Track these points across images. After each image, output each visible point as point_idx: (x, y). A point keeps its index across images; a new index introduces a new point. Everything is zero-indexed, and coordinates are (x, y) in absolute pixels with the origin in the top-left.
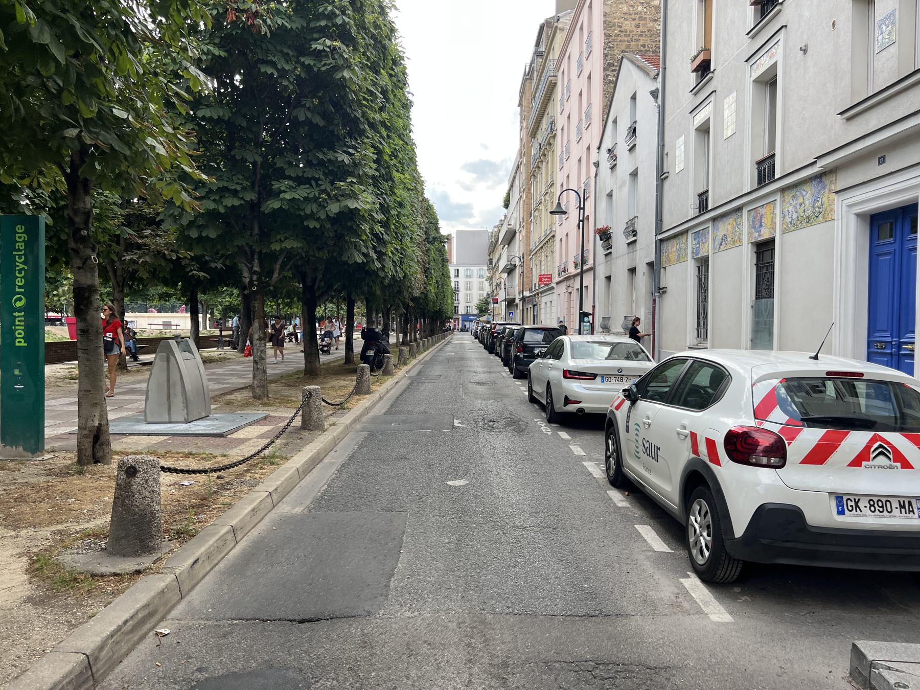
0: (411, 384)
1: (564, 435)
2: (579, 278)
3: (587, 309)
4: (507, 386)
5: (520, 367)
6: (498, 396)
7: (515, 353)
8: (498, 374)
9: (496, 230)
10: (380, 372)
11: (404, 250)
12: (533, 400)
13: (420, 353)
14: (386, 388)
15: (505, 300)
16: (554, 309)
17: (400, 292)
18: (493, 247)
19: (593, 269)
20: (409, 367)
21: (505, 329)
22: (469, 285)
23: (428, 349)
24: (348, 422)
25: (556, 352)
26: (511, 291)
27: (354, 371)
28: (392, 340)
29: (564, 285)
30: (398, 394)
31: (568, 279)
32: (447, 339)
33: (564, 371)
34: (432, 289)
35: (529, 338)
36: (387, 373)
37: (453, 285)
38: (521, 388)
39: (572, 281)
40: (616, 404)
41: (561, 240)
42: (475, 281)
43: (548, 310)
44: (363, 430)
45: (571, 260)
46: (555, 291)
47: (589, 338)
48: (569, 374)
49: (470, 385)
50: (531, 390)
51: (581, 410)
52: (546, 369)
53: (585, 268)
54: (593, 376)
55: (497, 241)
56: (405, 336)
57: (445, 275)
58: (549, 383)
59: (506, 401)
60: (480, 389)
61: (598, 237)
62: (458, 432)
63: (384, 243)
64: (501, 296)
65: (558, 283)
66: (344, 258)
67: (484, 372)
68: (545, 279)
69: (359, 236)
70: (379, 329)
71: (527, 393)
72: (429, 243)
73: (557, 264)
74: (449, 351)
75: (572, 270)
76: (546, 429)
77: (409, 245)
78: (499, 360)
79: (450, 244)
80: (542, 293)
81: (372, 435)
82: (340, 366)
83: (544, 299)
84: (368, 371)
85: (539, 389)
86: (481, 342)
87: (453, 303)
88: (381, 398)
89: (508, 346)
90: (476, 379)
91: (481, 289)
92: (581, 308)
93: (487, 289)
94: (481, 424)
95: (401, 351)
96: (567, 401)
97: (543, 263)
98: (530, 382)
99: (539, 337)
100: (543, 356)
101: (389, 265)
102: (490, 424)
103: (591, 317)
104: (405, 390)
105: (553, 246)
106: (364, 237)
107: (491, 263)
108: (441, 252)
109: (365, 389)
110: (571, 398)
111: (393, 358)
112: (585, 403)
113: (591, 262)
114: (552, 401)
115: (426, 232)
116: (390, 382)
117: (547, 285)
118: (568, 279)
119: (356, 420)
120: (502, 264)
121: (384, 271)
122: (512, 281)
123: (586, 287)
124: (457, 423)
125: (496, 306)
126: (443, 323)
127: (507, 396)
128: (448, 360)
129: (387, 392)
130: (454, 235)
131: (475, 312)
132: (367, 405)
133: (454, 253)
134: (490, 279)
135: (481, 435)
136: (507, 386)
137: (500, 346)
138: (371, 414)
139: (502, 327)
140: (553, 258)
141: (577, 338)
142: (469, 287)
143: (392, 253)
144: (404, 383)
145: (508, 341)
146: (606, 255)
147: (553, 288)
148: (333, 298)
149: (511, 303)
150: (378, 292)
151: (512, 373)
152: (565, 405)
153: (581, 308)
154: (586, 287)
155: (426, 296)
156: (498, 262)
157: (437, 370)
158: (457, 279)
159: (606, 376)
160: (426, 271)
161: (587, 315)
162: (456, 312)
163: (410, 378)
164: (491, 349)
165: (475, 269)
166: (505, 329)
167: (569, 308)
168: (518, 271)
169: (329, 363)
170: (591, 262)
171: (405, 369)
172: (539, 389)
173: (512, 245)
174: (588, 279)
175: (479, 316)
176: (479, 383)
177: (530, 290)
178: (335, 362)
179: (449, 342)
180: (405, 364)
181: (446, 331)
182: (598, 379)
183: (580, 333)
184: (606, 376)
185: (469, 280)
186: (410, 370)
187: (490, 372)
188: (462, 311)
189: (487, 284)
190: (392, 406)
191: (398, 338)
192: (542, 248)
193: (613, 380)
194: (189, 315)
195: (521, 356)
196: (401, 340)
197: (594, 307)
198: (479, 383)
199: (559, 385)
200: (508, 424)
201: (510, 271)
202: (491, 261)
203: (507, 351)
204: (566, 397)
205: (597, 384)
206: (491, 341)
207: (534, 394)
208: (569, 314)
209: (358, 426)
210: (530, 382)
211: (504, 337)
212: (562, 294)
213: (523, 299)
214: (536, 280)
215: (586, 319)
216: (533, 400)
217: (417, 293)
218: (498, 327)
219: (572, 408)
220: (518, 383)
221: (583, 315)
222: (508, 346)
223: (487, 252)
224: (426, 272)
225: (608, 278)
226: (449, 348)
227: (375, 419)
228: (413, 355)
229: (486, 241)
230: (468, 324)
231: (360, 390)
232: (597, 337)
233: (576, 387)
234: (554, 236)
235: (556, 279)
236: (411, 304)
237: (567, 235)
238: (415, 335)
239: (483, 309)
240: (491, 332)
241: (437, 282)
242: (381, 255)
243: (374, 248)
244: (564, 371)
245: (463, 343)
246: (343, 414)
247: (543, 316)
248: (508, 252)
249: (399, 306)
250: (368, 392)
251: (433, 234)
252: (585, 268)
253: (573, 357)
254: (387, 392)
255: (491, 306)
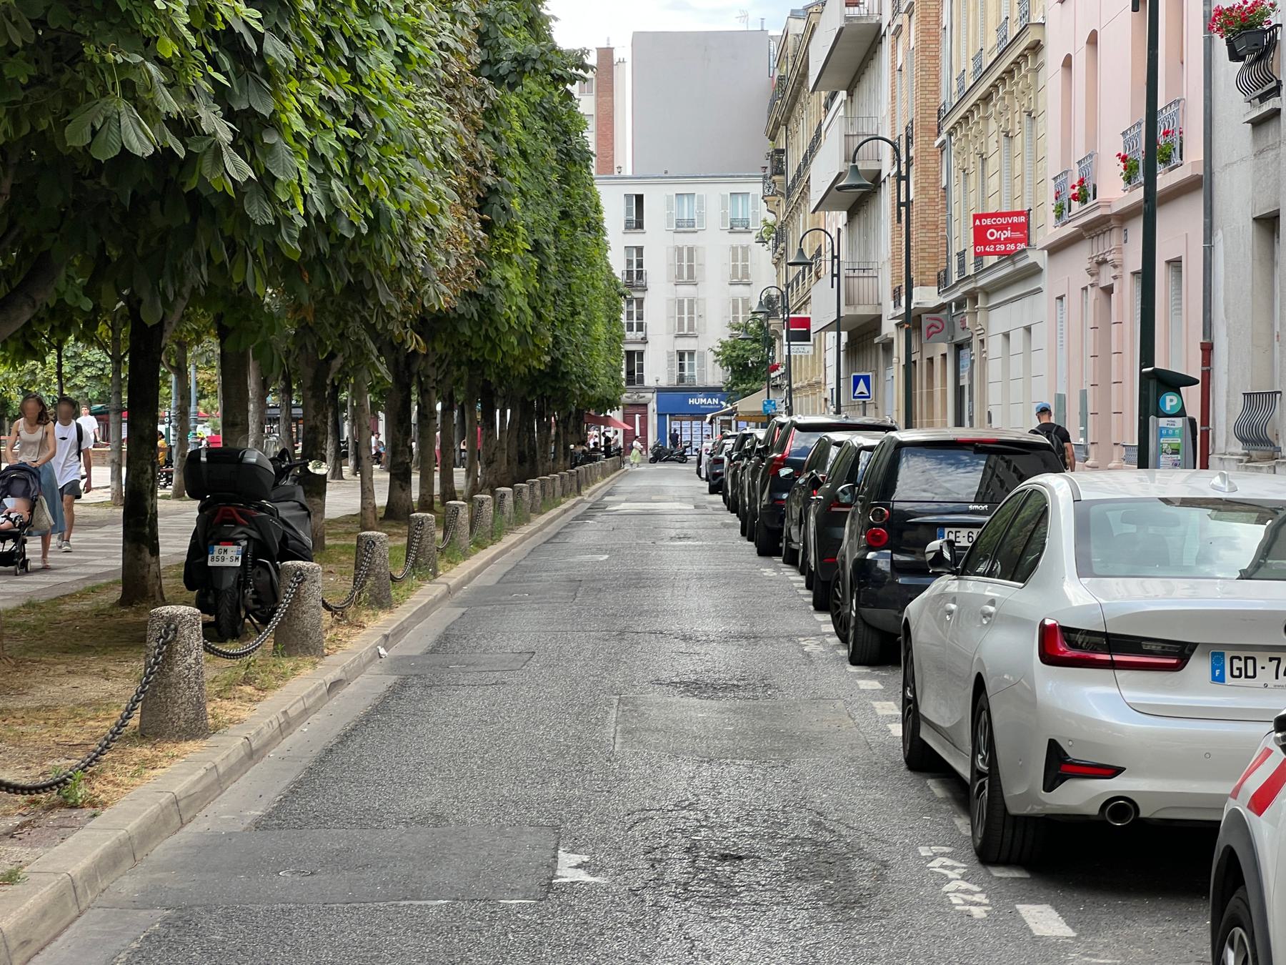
0: (396, 691)
1: (1044, 919)
2: (1136, 230)
3: (1176, 354)
4: (816, 700)
5: (879, 616)
6: (774, 741)
7: (851, 547)
8: (785, 648)
9: (799, 26)
10: (266, 639)
11: (368, 107)
12: (921, 759)
13: (453, 552)
14: (275, 712)
15: (837, 325)
16: (1040, 361)
17: (359, 291)
18: (787, 98)
19: (1201, 185)
20: (400, 615)
21: (824, 447)
22: (685, 264)
23: (495, 536)
24: (78, 867)
25: (1014, 549)
26: (862, 286)
27: (134, 638)
28: (341, 499)
29: (1081, 257)
30: (330, 737)
31: (1096, 228)
32: (590, 494)
33: (1047, 634)
34: (514, 279)
35: (918, 485)
36: (297, 643)
37: (617, 263)
38: (875, 702)
39: (1114, 239)
40: (1255, 783)
41: (1067, 63)
42: (715, 247)
43: (1016, 364)
44: (145, 902)
45: (1111, 146)
46: (1043, 282)
47: (1174, 481)
48: (1066, 647)
49: (655, 695)
50: (912, 715)
51: (1121, 807)
52: (973, 621)
53: (1164, 180)
54: (1175, 655)
55: (804, 75)
56: (400, 478)
57: (579, 218)
58: (979, 684)
59: (804, 764)
60: (699, 711)
61: (1221, 45)
62: (567, 908)
63: (268, 74)
64: (822, 306)
65: (1055, 249)
66: (76, 136)
67: (727, 639)
68: (1002, 232)
69: (148, 44)
70: (260, 451)
71: (897, 730)
72: (497, 80)
73: (1052, 166)
74: (589, 547)
75: (1116, 193)
76: (963, 889)
77: (399, 90)
78: (799, 580)
79: (606, 88)
80: (988, 291)
81: (183, 921)
82: (99, 613)
83: (1000, 319)
84: (194, 638)
85: (945, 710)
86: (732, 506)
87: (617, 339)
88: (252, 755)
89: (830, 520)
90: (688, 667)
91: (741, 278)
92: (1147, 353)
93: (765, 275)
94: (678, 869)
95: (364, 550)
96: (1060, 765)
97: (993, 164)
98: (909, 681)
99: (964, 481)
100: (963, 564)
101: (292, 168)
102: (717, 870)
103: (1191, 396)
104: (367, 718)
105: (1033, 88)
106: (168, 49)
107: (779, 170)
108: (560, 123)
109: (181, 713)
110: (1074, 753)
111: (321, 579)
112: (1139, 773)
113: (1194, 154)
114: (993, 762)
115: (482, 38)
116: (303, 681)
117: (1009, 256)
118: (1096, 228)
119: (113, 861)
120: (825, 171)
121: (270, 196)
122: (863, 241)
123: (1175, 264)
124: (569, 868)
125: (799, 349)
126: (576, 423)
127: (809, 743)
128: (575, 584)
129: (287, 726)
130: (623, 52)
131: (715, 375)
132: (180, 786)
133: (624, 137)
134: (777, 235)
135: (669, 924)
136: (816, 700)
137: (802, 521)
138: (201, 825)
139: (812, 440)
140: (1034, 140)
141: (1129, 483)
142: (686, 269)
143: (307, 117)
144: (368, 687)
145: (833, 499)
146: (1257, 123)
147: (1034, 271)
148: (91, 324)
149: (861, 338)
150: (269, 295)
151: (844, 640)
152: (1050, 785)
153: (1147, 353)
154: (1175, 264)
155: (487, 310)
156: (807, 161)
157: (521, 629)
158: (635, 239)
159: (1234, 656)
160: (485, 202)
161: (1174, 382)
162: (634, 377)
163: (398, 664)
164: (767, 536)
165: (713, 196)
166: (824, 447)
167: (1103, 355)
168: (887, 196)
169: (61, 599)
170: (1194, 154)
171: (379, 623)
172: (945, 710)
173: (864, 86)
174: (1178, 231)
175: (730, 393)
176: (695, 687)
177: (942, 281)
178: (82, 595)
179: (597, 507)
180: (381, 602)
181: (590, 457)
182: (1199, 667)
183: (1143, 463)
184: (1234, 656)
185: (685, 240)
186: (400, 631)
187: (753, 638)
188: (657, 371)
189: (762, 257)
190: (295, 791)
191: (367, 492)
192: (986, 99)
193: (1266, 672)
194: (387, 476)
195: (884, 565)
196: (381, 499)
197: (1207, 349)
198: (695, 687)
199: (1028, 699)
200: (796, 873)
201: (857, 196)
202: (778, 160)
203: (828, 543)
204: (1054, 746)
205: (1194, 687)
206: (770, 502)
207: (926, 735)
208: (1103, 382)
209: (128, 884)
210: (909, 681)
211: (815, 484)
212: (1074, 298)
213: (912, 321)
214: (962, 238)
215: (1170, 402)
216: (921, 759)
217: (441, 296)
218: (797, 442)
219: (1081, 796)
220: (869, 682)
221: (1155, 385)
222: (830, 520)
223: (762, 122)
224: (483, 204)
225: (1268, 223)
226: (590, 533)
227: (211, 846)
228: (421, 563)
229: (758, 77)
230: (689, 431)
231: (162, 717)
232: (1209, 483)
233: (1098, 705)
234: (1036, 48)
235: (1047, 230)
236: (414, 342)
237: (1093, 40)
238: (447, 479)
239: (749, 365)
240: (765, 459)
241: (537, 248)
242: (251, 131)
243: (221, 95)
244: (1047, 634)
245: (663, 509)
246: (64, 830)
247: (994, 395)
248: (850, 119)
249: (360, 349)
250: (197, 729)
251: (515, 43)
252: (1164, 180)
253: (1084, 569)
254: (287, 726)
255: (781, 351)
